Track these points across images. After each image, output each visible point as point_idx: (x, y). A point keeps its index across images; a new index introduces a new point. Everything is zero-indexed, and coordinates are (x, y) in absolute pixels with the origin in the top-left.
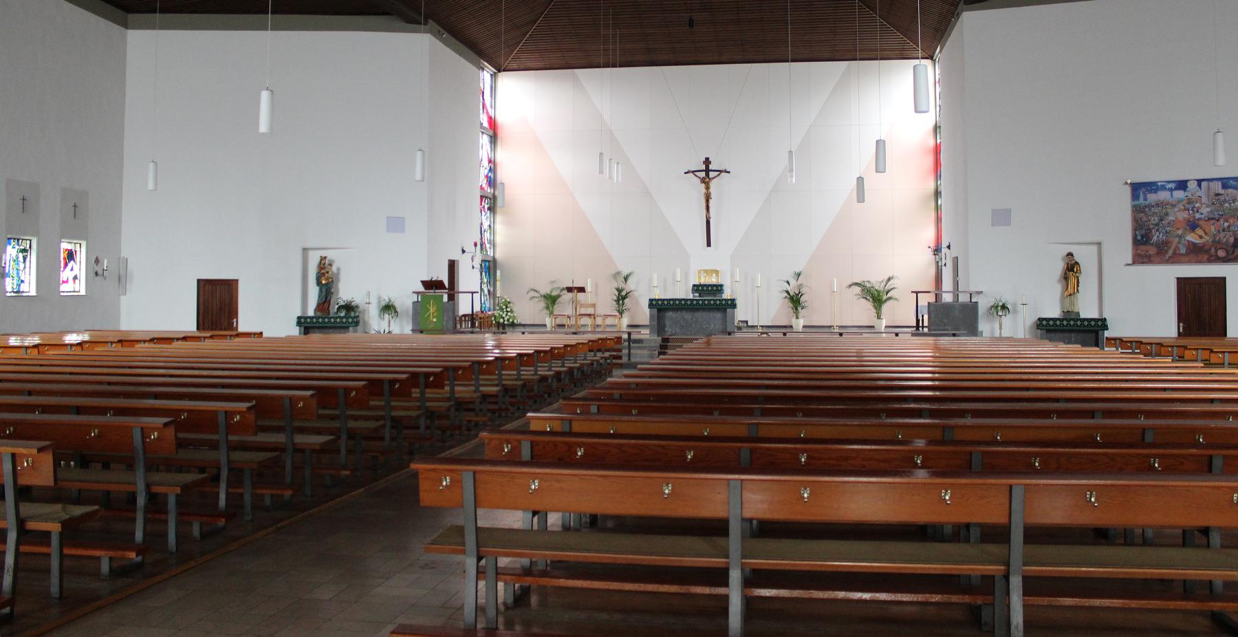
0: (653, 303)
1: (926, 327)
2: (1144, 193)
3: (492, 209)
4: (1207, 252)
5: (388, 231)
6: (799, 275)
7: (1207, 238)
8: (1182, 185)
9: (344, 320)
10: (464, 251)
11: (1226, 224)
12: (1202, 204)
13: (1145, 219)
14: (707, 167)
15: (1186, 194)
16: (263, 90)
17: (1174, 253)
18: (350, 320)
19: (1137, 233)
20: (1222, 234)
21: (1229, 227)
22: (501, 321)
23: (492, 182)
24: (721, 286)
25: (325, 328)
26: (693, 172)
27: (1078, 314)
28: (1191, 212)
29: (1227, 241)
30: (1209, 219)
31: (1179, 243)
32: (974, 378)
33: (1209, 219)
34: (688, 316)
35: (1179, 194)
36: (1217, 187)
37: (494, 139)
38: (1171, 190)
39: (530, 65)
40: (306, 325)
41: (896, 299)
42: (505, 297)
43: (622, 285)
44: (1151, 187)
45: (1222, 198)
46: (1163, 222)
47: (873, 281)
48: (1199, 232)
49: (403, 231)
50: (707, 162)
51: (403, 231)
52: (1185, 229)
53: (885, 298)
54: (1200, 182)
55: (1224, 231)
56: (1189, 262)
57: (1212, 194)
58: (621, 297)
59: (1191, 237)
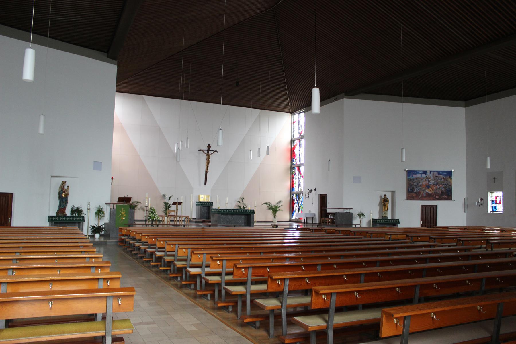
1: (146, 223)
2: (412, 174)
4: (433, 196)
5: (94, 169)
7: (433, 191)
8: (425, 172)
11: (439, 187)
12: (431, 179)
13: (412, 183)
15: (426, 175)
17: (422, 196)
19: (409, 188)
20: (438, 190)
21: (440, 188)
24: (212, 203)
25: (63, 223)
26: (203, 150)
28: (428, 182)
29: (439, 193)
30: (434, 185)
31: (423, 193)
32: (180, 242)
33: (434, 185)
34: (230, 217)
35: (424, 175)
36: (436, 174)
38: (421, 174)
41: (282, 210)
42: (153, 207)
44: (415, 172)
45: (438, 178)
46: (418, 185)
48: (430, 189)
49: (101, 170)
50: (209, 146)
51: (101, 170)
52: (426, 188)
54: (431, 172)
55: (438, 189)
57: (435, 176)
59: (427, 191)
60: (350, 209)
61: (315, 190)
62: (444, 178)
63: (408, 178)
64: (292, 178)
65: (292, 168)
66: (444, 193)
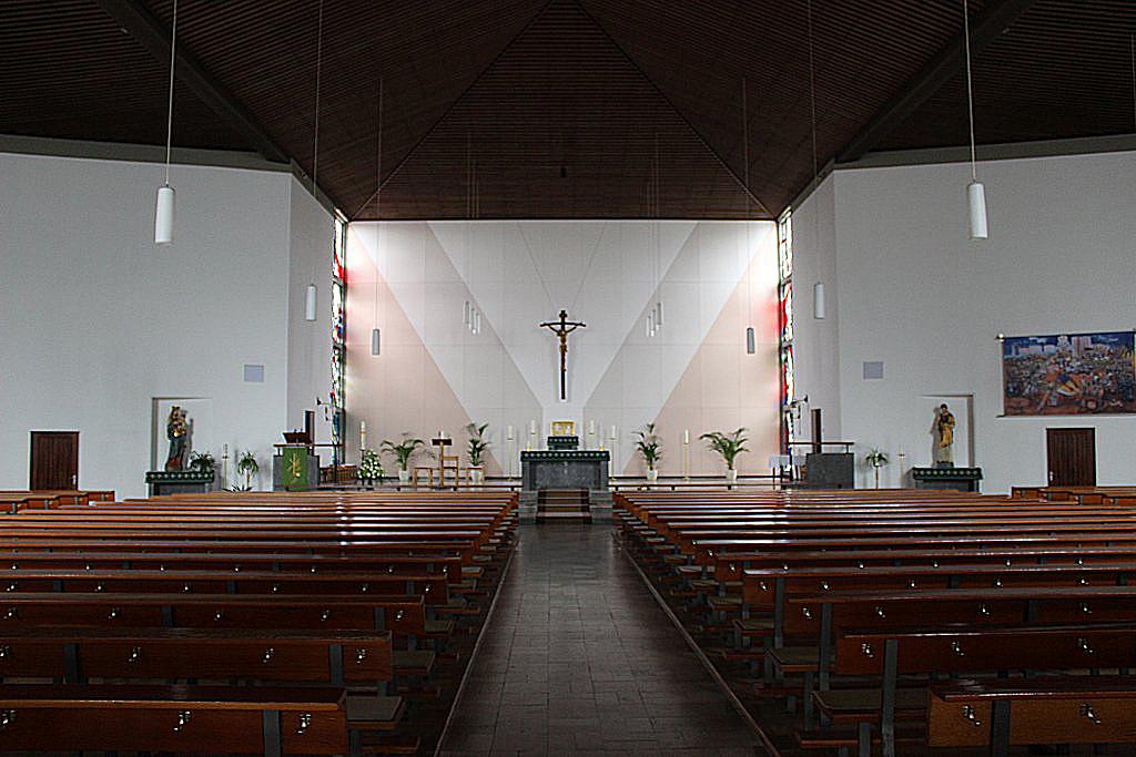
0: (525, 456)
3: (342, 361)
6: (652, 426)
8: (1053, 340)
9: (199, 476)
10: (319, 403)
11: (1096, 377)
14: (563, 320)
16: (162, 187)
18: (206, 476)
19: (1010, 385)
20: (1092, 386)
21: (1098, 379)
22: (369, 475)
23: (342, 333)
26: (549, 325)
27: (952, 464)
31: (1051, 394)
35: (1051, 348)
36: (1087, 341)
37: (344, 289)
38: (1042, 344)
39: (380, 215)
40: (157, 482)
43: (477, 438)
44: (1023, 341)
47: (725, 433)
50: (563, 315)
52: (1056, 382)
53: (736, 449)
54: (1070, 337)
55: (1094, 383)
56: (1060, 414)
57: (1082, 349)
58: (477, 449)
60: (848, 444)
61: (806, 400)
62: (1109, 353)
63: (1006, 357)
64: (783, 374)
65: (782, 349)
66: (1114, 394)
